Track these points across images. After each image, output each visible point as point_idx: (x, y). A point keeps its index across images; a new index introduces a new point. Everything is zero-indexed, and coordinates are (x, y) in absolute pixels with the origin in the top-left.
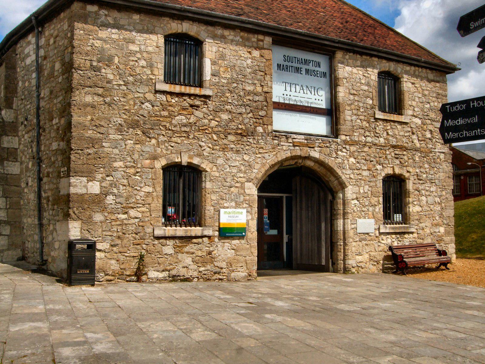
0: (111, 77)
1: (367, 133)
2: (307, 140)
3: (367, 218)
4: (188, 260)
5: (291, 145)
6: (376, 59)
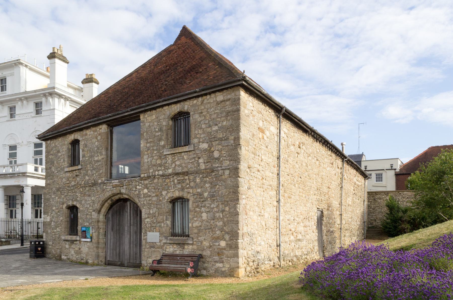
1: (159, 168)
2: (119, 182)
3: (155, 231)
5: (112, 187)
6: (167, 107)
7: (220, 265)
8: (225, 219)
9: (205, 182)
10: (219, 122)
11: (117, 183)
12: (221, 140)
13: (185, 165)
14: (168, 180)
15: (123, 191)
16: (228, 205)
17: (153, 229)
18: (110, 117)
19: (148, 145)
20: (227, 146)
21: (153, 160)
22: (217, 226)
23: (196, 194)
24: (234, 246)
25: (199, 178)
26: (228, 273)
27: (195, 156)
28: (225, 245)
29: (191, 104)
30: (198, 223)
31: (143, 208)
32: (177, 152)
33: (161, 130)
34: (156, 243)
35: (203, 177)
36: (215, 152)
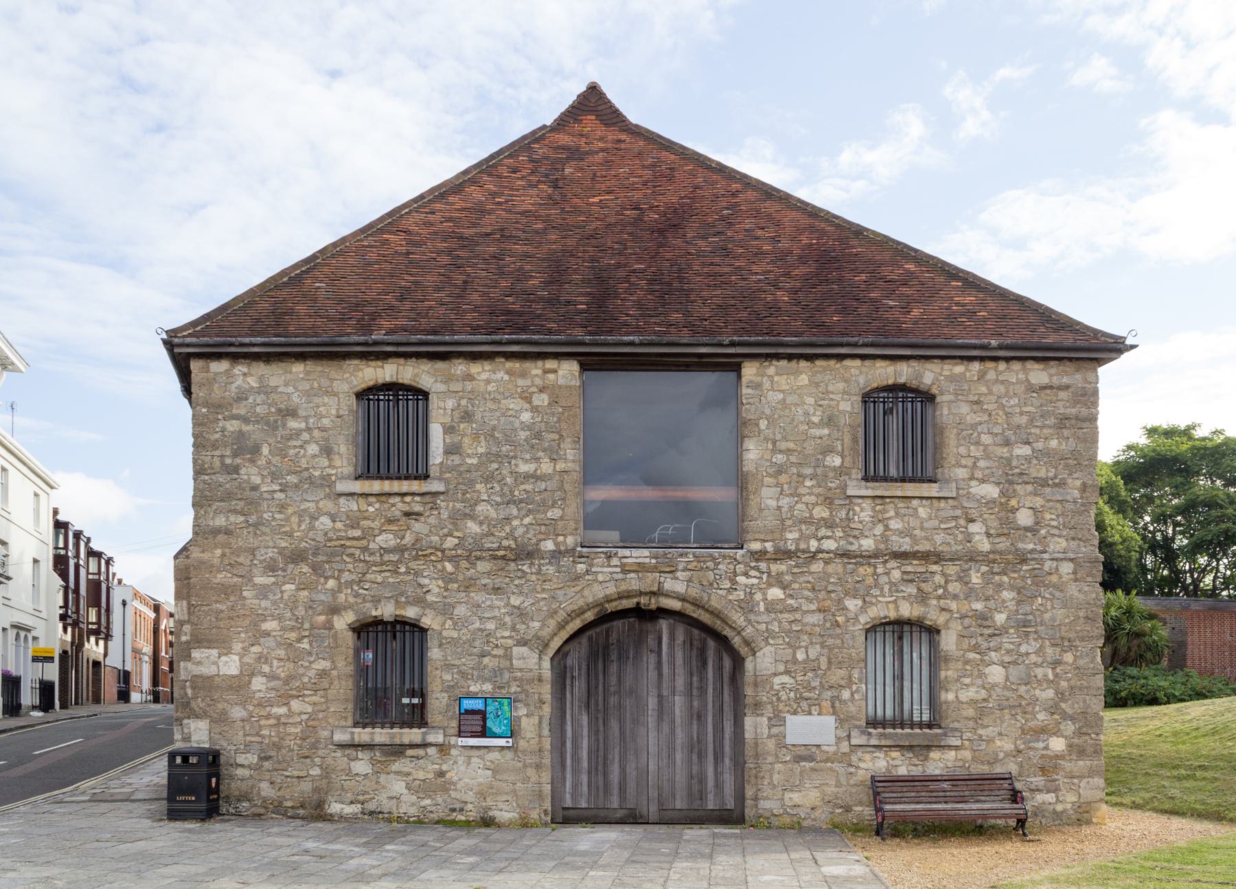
0: (257, 480)
4: (399, 787)
5: (618, 570)
6: (858, 362)
7: (1050, 797)
8: (1064, 684)
9: (1000, 586)
10: (1038, 437)
11: (647, 560)
12: (1044, 483)
13: (923, 534)
14: (870, 570)
15: (669, 584)
16: (1072, 647)
17: (810, 706)
18: (632, 344)
19: (780, 458)
20: (1060, 501)
21: (799, 506)
22: (1037, 700)
23: (970, 614)
24: (1090, 750)
25: (979, 575)
26: (1073, 817)
27: (958, 512)
28: (1064, 748)
29: (946, 373)
30: (977, 692)
31: (768, 644)
32: (899, 493)
33: (830, 421)
34: (818, 746)
35: (993, 573)
36: (1023, 511)
